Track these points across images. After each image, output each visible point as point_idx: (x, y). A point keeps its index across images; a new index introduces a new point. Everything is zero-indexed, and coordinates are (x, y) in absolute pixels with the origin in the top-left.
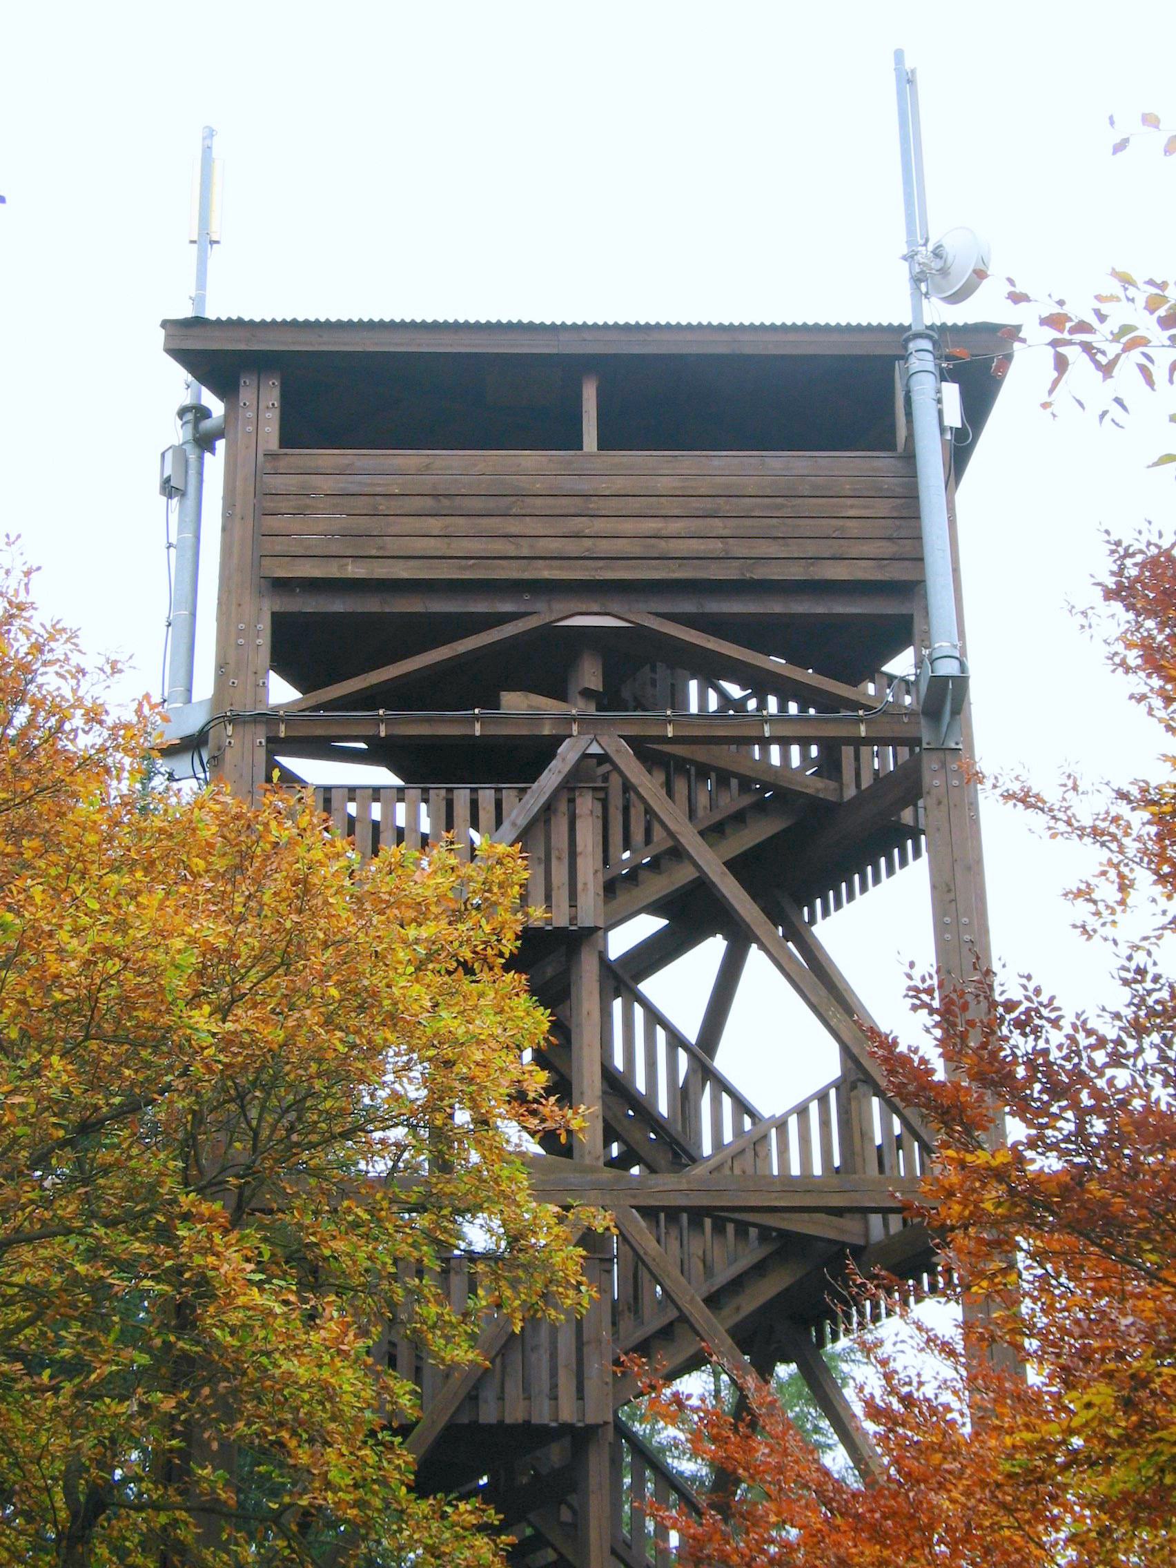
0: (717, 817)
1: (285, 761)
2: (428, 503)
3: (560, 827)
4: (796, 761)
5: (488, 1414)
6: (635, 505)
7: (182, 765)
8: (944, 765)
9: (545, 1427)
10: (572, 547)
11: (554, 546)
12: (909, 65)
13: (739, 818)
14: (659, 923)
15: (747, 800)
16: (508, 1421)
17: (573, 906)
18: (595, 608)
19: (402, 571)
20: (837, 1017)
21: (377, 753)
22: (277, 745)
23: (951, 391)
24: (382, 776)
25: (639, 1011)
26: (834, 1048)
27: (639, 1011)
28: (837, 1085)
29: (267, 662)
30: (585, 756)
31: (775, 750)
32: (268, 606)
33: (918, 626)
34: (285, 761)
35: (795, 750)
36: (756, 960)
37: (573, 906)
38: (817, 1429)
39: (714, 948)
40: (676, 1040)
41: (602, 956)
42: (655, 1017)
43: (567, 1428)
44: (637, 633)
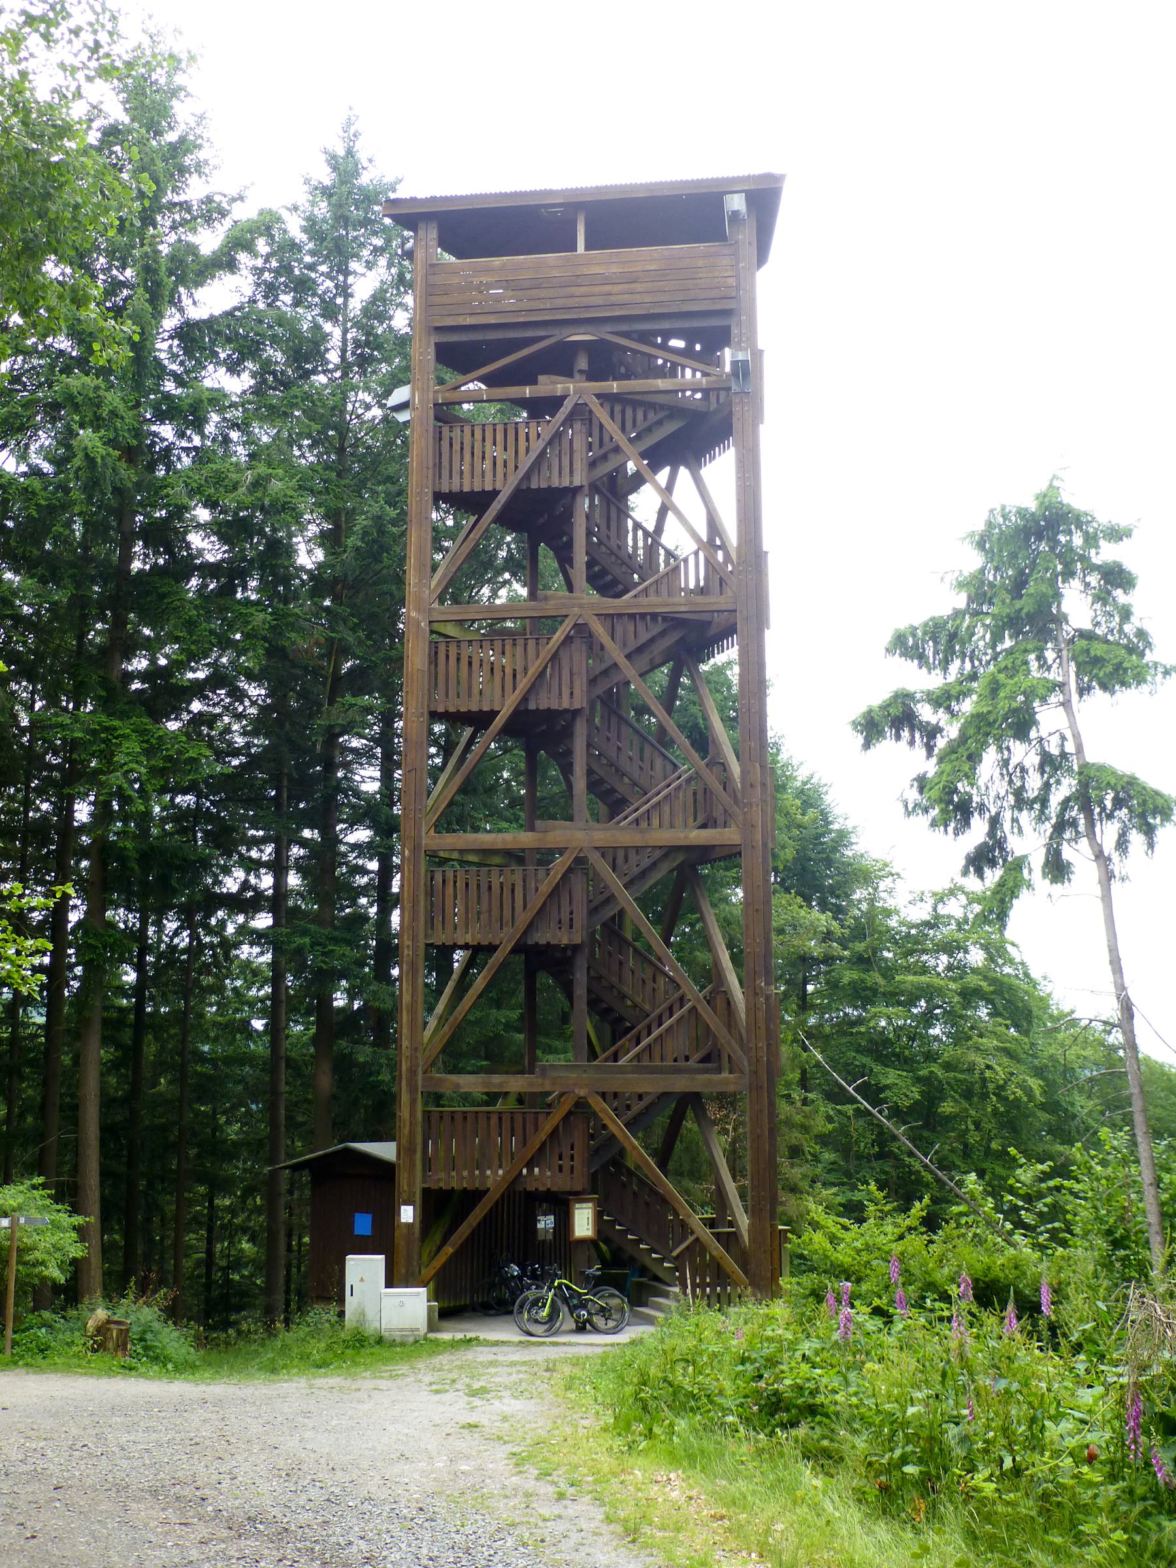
5: (532, 706)
8: (742, 401)
9: (557, 711)
11: (560, 303)
12: (356, 127)
16: (485, 709)
18: (582, 331)
30: (576, 404)
33: (735, 331)
40: (646, 534)
43: (566, 711)
44: (602, 341)
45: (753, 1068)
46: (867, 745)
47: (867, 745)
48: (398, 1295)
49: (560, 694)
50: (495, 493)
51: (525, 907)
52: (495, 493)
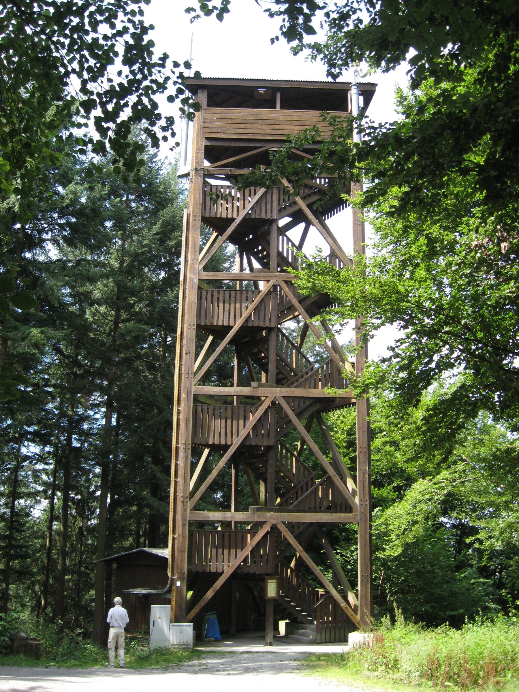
0: (305, 195)
1: (207, 180)
2: (241, 121)
3: (269, 196)
4: (323, 183)
6: (288, 122)
7: (184, 180)
10: (273, 132)
11: (269, 131)
13: (309, 195)
14: (290, 219)
15: (311, 191)
17: (271, 214)
19: (235, 137)
20: (330, 240)
21: (228, 178)
22: (206, 176)
23: (361, 98)
24: (227, 183)
25: (285, 238)
26: (329, 247)
27: (285, 238)
28: (329, 256)
29: (203, 155)
31: (318, 180)
32: (205, 143)
34: (207, 180)
35: (323, 180)
36: (312, 228)
37: (271, 214)
38: (8, 204)
39: (302, 225)
40: (293, 245)
41: (278, 225)
42: (289, 240)
45: (363, 510)
46: (376, 85)
47: (376, 85)
48: (180, 626)
49: (265, 319)
50: (233, 220)
51: (244, 426)
52: (233, 220)
